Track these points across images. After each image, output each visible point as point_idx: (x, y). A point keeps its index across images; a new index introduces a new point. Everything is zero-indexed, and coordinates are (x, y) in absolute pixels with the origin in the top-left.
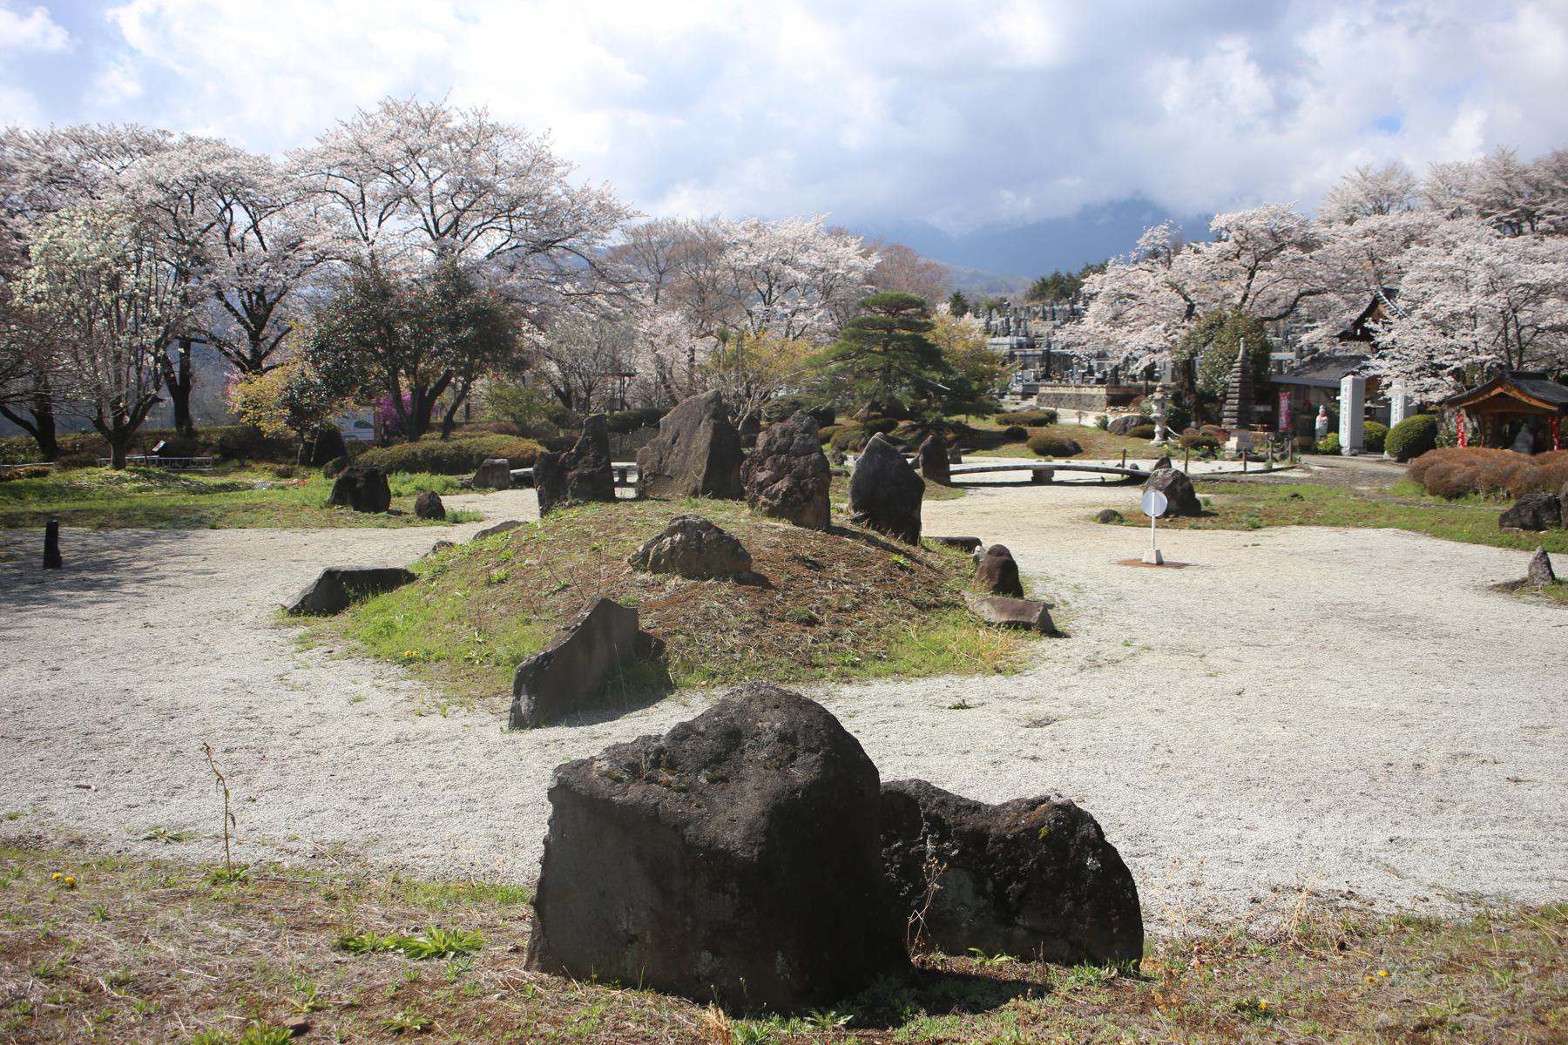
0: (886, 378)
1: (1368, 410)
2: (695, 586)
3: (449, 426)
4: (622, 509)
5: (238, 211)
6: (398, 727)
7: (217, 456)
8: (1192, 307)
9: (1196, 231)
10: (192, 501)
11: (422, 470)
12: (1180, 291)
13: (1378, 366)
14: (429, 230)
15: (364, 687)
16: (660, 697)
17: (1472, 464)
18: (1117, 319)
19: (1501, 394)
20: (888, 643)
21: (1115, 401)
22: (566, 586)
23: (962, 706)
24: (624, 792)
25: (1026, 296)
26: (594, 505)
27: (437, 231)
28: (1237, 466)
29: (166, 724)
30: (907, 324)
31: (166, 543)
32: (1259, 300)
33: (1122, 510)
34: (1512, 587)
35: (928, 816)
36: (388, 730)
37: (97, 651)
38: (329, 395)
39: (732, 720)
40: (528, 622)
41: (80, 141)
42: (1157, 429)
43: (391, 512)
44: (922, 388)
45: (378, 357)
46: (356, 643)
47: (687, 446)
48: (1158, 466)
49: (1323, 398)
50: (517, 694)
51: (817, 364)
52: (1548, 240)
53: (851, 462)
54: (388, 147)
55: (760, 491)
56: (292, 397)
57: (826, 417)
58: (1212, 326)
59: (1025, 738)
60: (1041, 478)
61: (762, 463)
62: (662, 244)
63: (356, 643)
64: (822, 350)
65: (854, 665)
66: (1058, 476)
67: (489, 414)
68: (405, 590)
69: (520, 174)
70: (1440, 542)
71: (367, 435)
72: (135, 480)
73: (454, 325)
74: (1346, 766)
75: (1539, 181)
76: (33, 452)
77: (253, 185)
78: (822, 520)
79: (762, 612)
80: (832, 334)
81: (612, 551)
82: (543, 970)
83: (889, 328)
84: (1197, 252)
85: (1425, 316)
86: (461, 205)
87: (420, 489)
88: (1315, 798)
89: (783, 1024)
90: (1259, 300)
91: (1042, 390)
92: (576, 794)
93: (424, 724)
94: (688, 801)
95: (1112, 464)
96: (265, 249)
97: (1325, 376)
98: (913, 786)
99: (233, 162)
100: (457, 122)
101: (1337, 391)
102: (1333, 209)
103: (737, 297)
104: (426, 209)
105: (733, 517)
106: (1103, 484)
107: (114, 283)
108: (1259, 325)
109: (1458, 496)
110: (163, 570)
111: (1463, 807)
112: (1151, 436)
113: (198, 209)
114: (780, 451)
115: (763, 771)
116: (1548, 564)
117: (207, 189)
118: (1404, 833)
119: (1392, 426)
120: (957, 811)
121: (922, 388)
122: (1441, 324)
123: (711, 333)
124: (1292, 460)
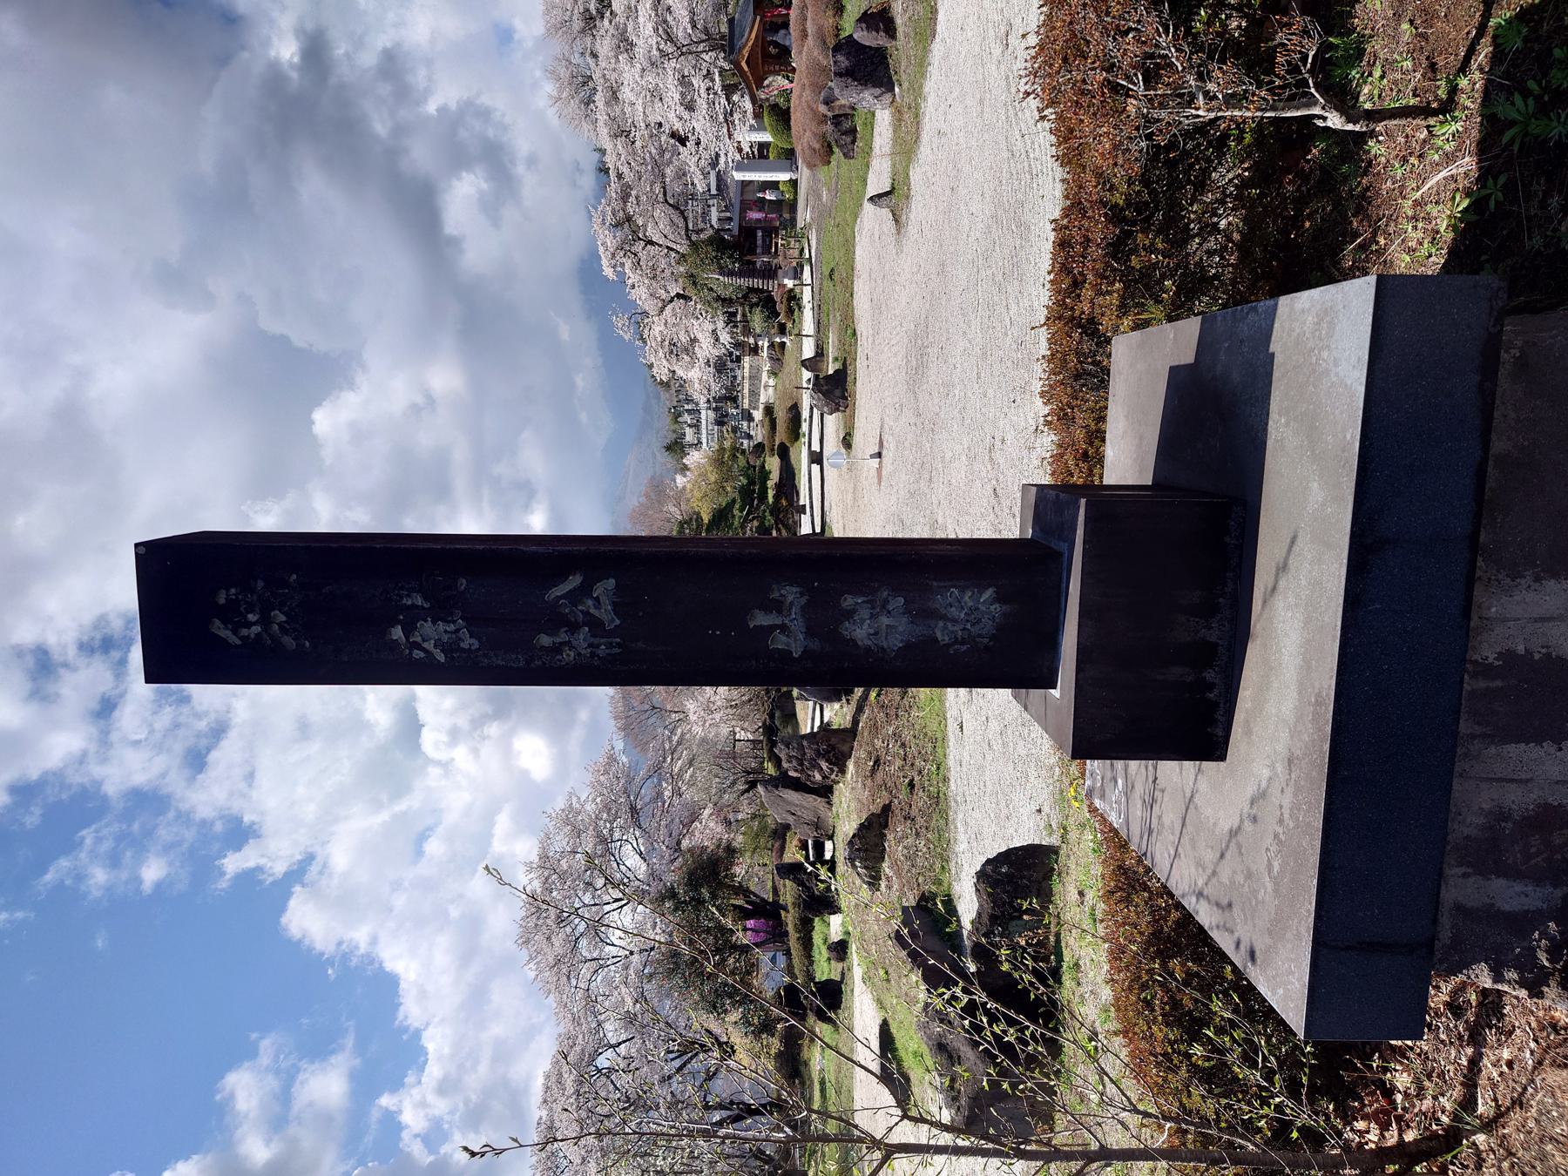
5: (602, 1062)
7: (797, 1081)
11: (811, 938)
14: (622, 907)
19: (747, 62)
25: (668, 391)
27: (621, 900)
42: (778, 340)
47: (797, 806)
54: (557, 944)
56: (753, 1032)
58: (695, 283)
66: (816, 447)
69: (578, 833)
78: (851, 733)
91: (746, 406)
96: (633, 1038)
97: (733, 193)
104: (607, 908)
112: (783, 344)
114: (802, 764)
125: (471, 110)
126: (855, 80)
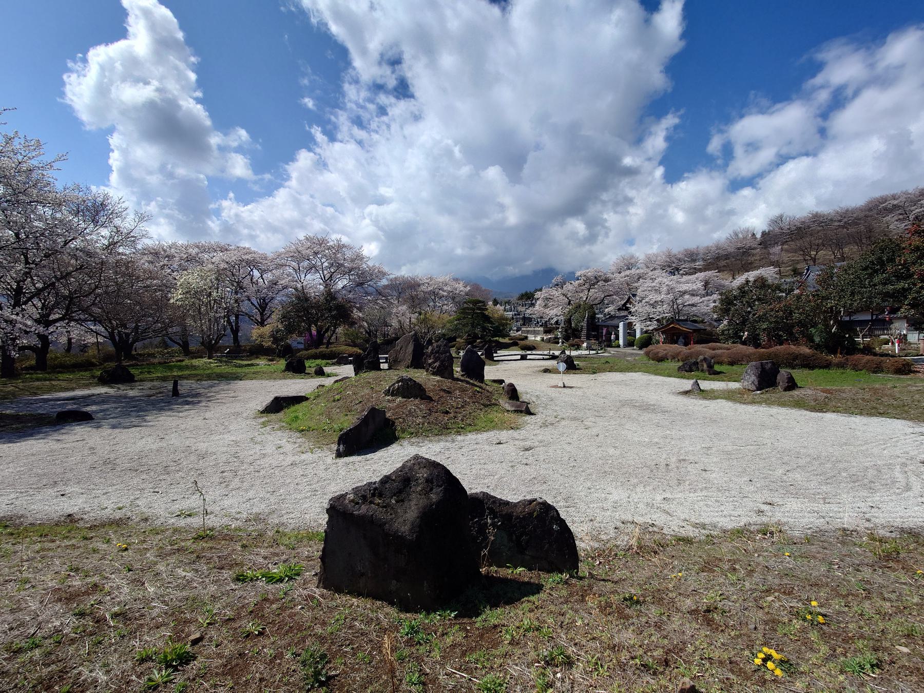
0: (473, 326)
1: (628, 333)
2: (406, 401)
3: (329, 343)
4: (382, 373)
6: (293, 459)
8: (570, 301)
9: (571, 277)
10: (235, 370)
12: (566, 297)
13: (632, 319)
15: (284, 442)
16: (392, 443)
17: (666, 350)
18: (546, 306)
20: (474, 419)
21: (547, 332)
22: (361, 402)
23: (500, 443)
24: (359, 509)
26: (373, 371)
28: (587, 352)
29: (200, 461)
30: (479, 309)
31: (223, 386)
32: (591, 299)
33: (550, 368)
34: (686, 393)
35: (488, 508)
36: (290, 459)
37: (182, 430)
38: (287, 333)
39: (406, 473)
40: (347, 415)
41: (198, 247)
42: (560, 341)
43: (306, 373)
44: (484, 329)
45: (304, 321)
46: (284, 424)
48: (561, 353)
49: (614, 329)
50: (339, 444)
51: (450, 322)
52: (684, 277)
53: (462, 354)
55: (430, 367)
57: (454, 339)
59: (523, 456)
60: (523, 358)
61: (430, 357)
62: (400, 284)
63: (284, 424)
64: (452, 317)
65: (462, 428)
66: (529, 357)
67: (343, 339)
68: (304, 404)
69: (353, 261)
70: (657, 377)
71: (302, 346)
72: (216, 363)
73: (330, 310)
74: (640, 466)
75: (680, 259)
76: (181, 353)
77: (261, 263)
79: (430, 410)
80: (455, 312)
81: (378, 389)
82: (325, 588)
83: (473, 310)
84: (571, 284)
85: (646, 302)
86: (332, 270)
87: (317, 365)
88: (631, 479)
89: (426, 617)
90: (591, 299)
91: (523, 329)
92: (338, 511)
93: (304, 456)
94: (387, 512)
95: (546, 352)
97: (614, 322)
98: (482, 495)
99: (253, 255)
100: (331, 243)
101: (618, 327)
102: (614, 269)
103: (425, 300)
105: (420, 376)
106: (543, 359)
107: (210, 295)
108: (591, 307)
109: (662, 361)
110: (219, 396)
111: (687, 483)
113: (241, 270)
114: (436, 352)
115: (419, 496)
116: (698, 385)
117: (244, 264)
118: (668, 495)
119: (637, 337)
120: (500, 505)
121: (484, 329)
122: (652, 305)
123: (416, 312)
124: (605, 350)
125: (607, 230)
126: (761, 372)
